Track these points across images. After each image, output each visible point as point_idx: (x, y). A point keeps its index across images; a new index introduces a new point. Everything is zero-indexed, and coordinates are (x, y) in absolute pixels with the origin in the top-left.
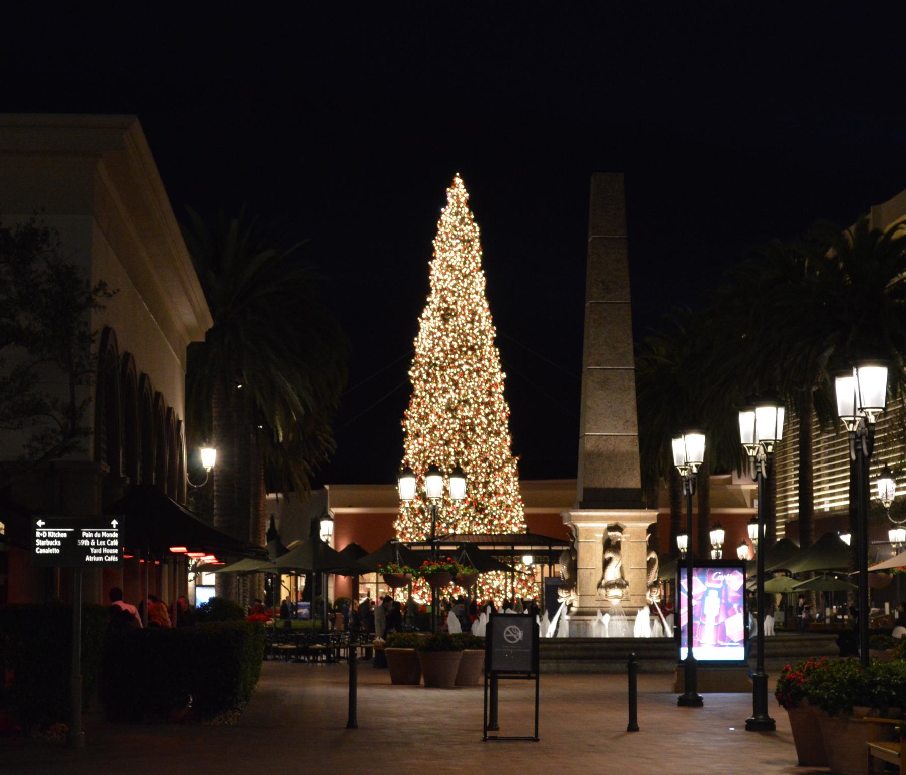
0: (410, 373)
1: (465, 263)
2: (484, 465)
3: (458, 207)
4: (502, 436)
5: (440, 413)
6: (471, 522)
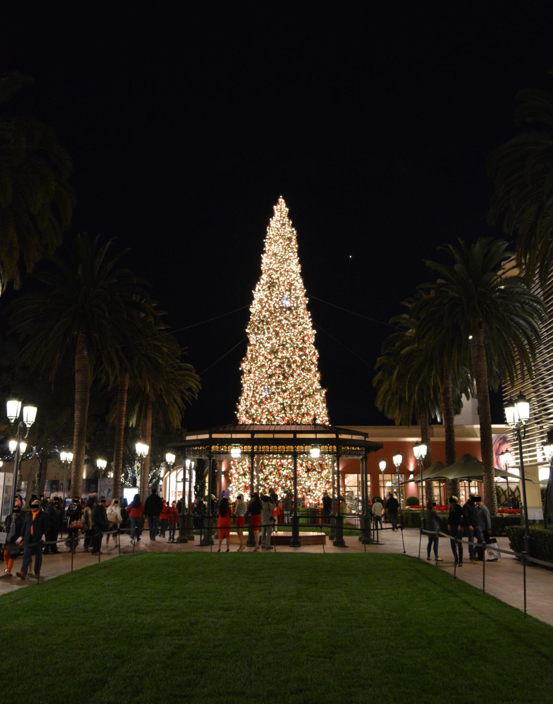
0: (247, 331)
4: (312, 372)
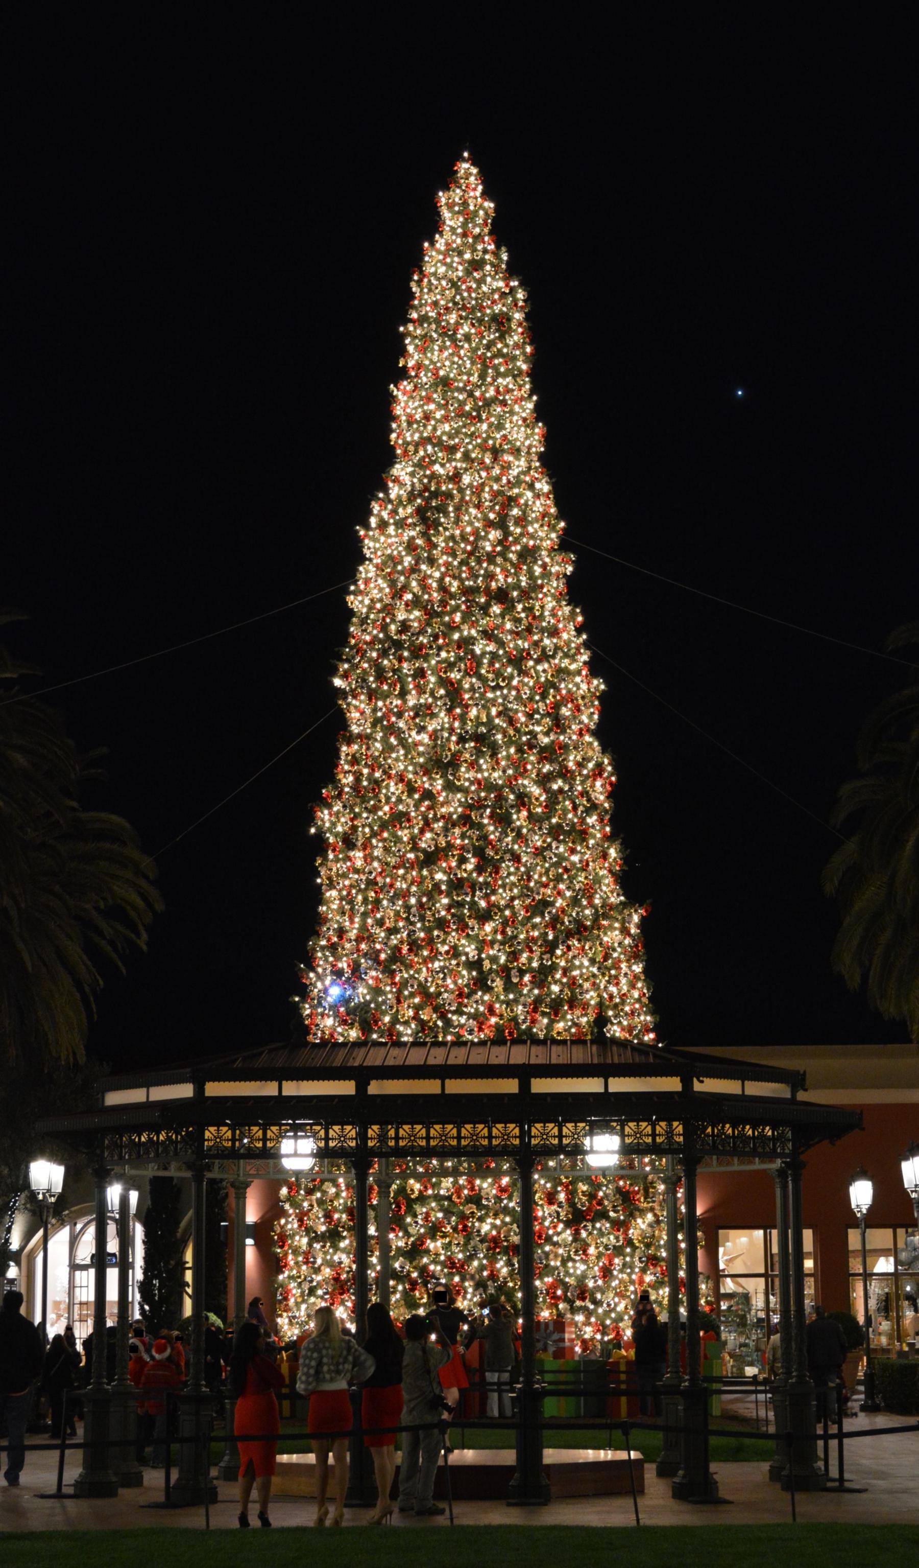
0: (338, 682)
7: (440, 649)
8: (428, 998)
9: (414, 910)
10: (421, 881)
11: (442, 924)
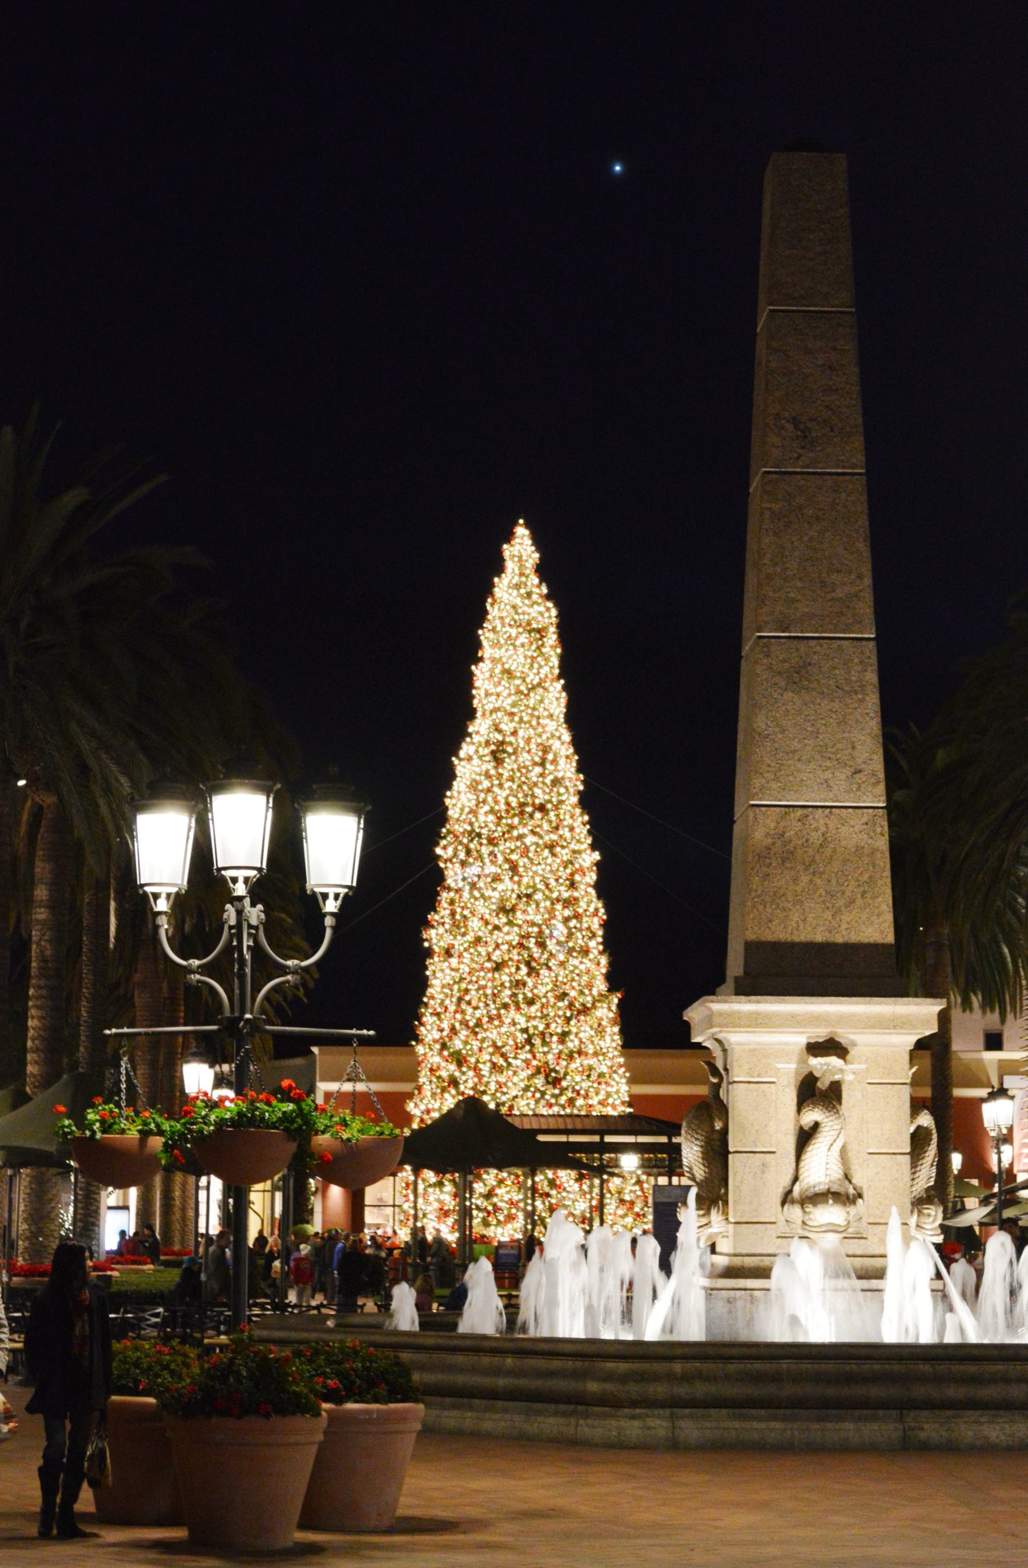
0: (439, 851)
1: (532, 666)
2: (560, 1004)
3: (521, 574)
4: (591, 956)
5: (487, 916)
6: (537, 1102)
7: (505, 840)
8: (497, 1048)
9: (489, 997)
10: (493, 980)
11: (506, 1006)
